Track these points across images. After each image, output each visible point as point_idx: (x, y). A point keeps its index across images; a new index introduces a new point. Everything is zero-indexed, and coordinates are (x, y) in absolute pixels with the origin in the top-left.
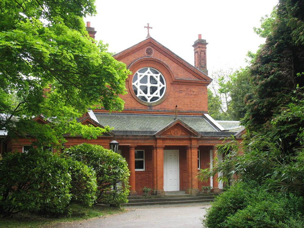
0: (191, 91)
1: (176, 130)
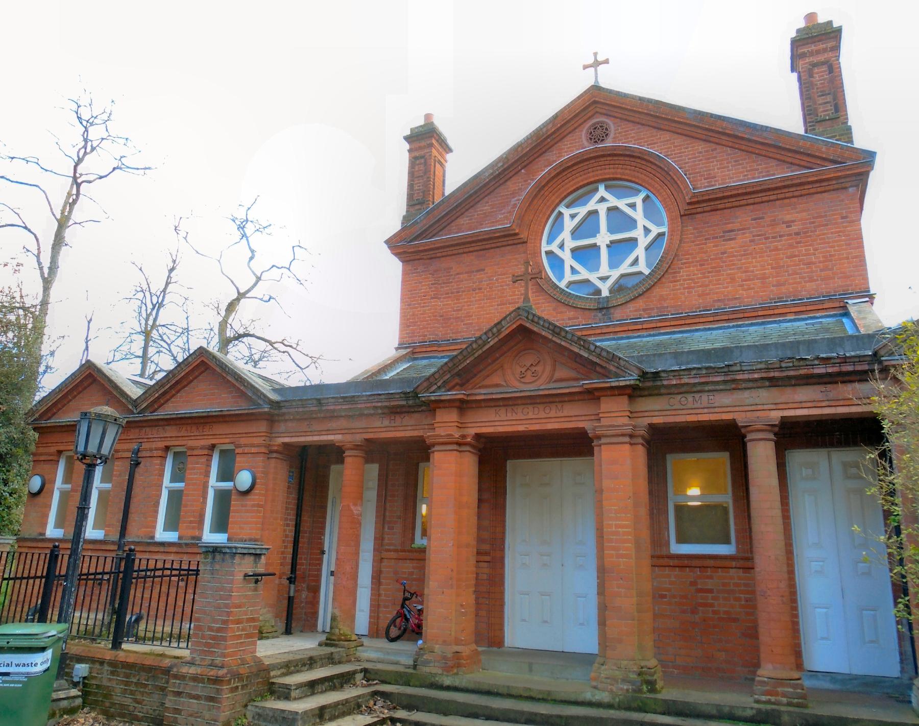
0: (774, 223)
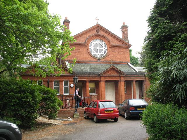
0: (120, 51)
1: (112, 71)
